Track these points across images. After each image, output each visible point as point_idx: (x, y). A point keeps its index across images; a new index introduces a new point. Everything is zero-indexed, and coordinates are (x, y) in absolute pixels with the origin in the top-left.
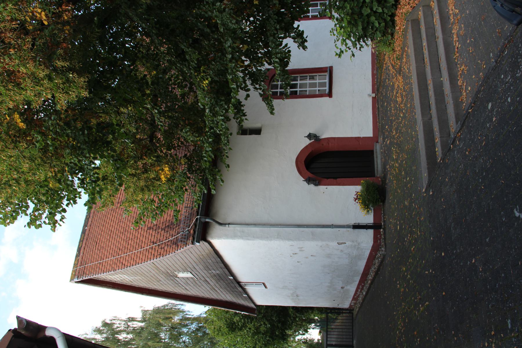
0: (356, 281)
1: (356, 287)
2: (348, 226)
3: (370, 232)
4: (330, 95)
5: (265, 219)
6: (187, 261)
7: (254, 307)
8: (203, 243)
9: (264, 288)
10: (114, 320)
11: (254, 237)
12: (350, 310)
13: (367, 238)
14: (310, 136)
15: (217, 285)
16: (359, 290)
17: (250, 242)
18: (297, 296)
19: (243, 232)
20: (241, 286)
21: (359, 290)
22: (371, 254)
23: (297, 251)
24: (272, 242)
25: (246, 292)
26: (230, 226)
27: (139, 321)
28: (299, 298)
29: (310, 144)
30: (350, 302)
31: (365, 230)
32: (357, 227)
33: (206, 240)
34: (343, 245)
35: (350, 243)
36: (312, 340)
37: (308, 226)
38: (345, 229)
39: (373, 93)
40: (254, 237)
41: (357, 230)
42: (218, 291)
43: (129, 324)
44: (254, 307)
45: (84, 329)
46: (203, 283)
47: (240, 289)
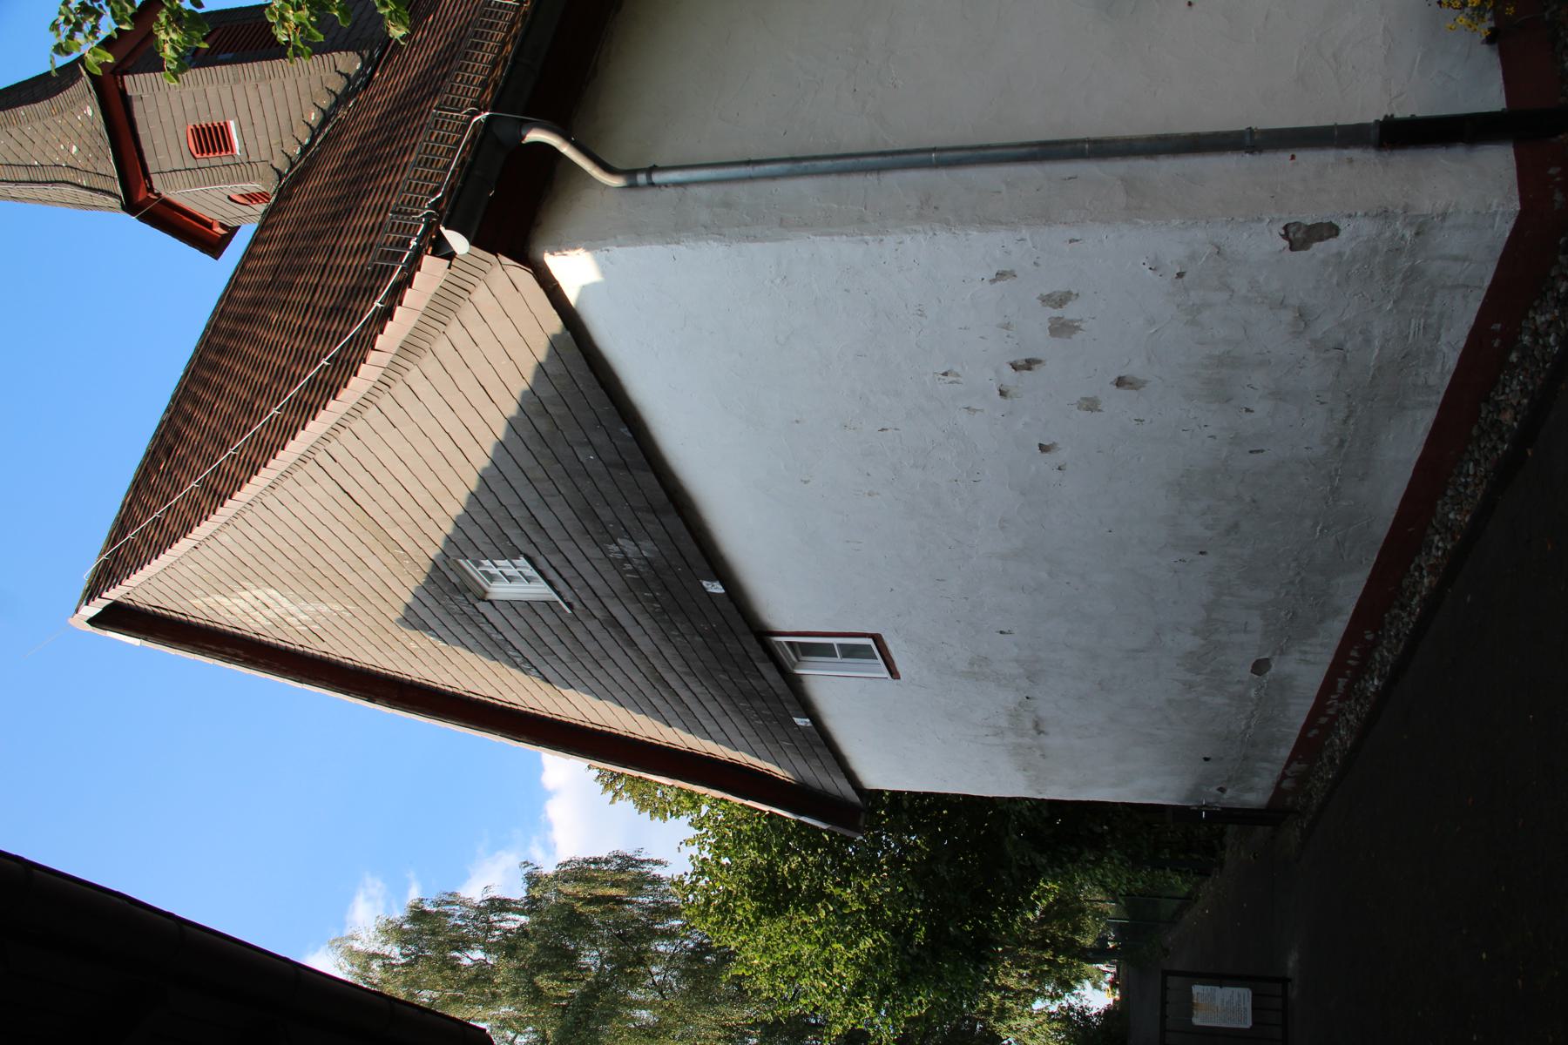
0: (1337, 612)
1: (1328, 658)
5: (856, 135)
6: (255, 341)
7: (856, 799)
9: (886, 674)
10: (448, 903)
11: (786, 223)
12: (1272, 815)
13: (1475, 199)
15: (668, 652)
16: (1341, 682)
17: (762, 255)
18: (1038, 728)
19: (727, 205)
20: (771, 654)
21: (1341, 682)
22: (1478, 335)
23: (1037, 339)
24: (890, 240)
25: (808, 709)
26: (657, 178)
27: (521, 912)
28: (1043, 739)
30: (1278, 769)
31: (1459, 151)
32: (1398, 134)
35: (1368, 228)
36: (1082, 1013)
38: (1329, 155)
40: (782, 223)
41: (1403, 161)
42: (694, 706)
43: (493, 918)
44: (856, 799)
45: (339, 933)
46: (601, 635)
47: (772, 676)
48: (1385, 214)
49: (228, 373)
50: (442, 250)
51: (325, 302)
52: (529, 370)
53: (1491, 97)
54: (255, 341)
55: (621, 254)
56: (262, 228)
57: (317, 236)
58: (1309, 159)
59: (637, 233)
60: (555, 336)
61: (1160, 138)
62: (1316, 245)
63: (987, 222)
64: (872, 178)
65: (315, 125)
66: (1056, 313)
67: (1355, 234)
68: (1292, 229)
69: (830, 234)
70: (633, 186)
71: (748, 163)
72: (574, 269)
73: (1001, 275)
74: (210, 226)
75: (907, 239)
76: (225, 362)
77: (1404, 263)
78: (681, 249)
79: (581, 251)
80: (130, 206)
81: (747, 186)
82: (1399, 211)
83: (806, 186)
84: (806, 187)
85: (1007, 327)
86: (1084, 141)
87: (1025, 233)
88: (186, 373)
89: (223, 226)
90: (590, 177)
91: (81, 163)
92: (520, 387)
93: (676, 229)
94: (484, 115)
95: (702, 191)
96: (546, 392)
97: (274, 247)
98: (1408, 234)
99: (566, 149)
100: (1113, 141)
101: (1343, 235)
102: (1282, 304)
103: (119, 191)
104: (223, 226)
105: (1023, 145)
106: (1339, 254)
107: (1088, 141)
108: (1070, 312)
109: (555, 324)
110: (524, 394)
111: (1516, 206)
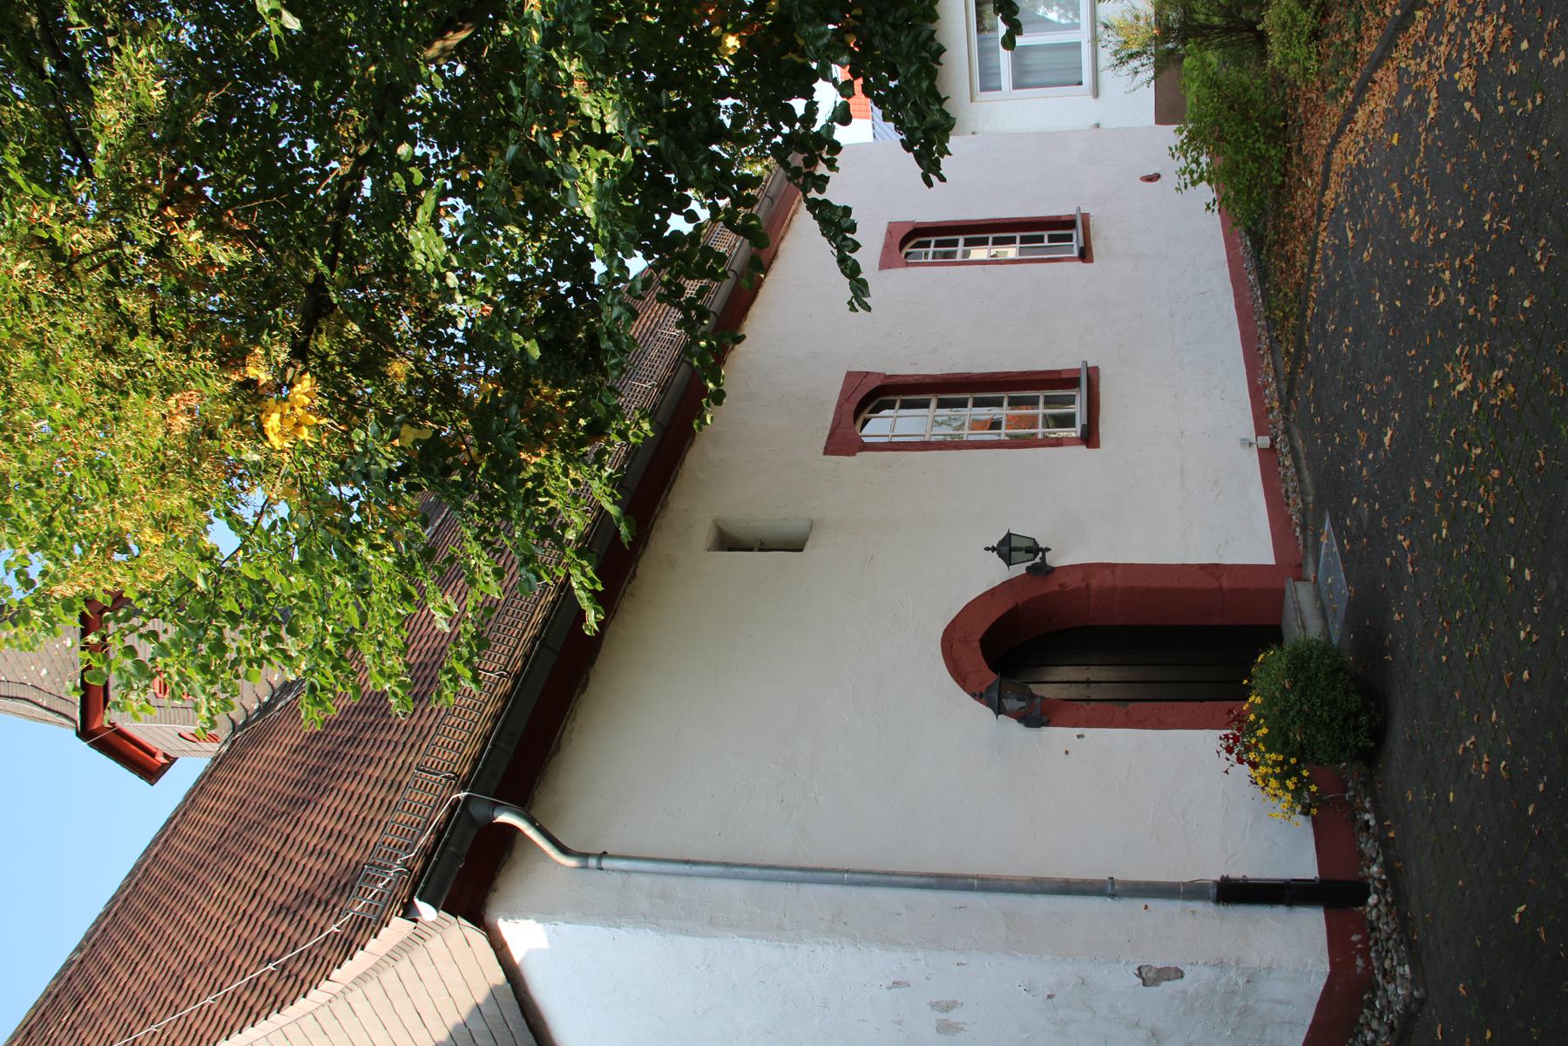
2: (1192, 891)
3: (1311, 922)
4: (1090, 438)
5: (781, 849)
6: (192, 907)
8: (461, 932)
11: (716, 922)
13: (1295, 949)
14: (1007, 549)
17: (692, 946)
26: (606, 863)
29: (1008, 585)
31: (1281, 910)
32: (1233, 892)
33: (477, 917)
34: (1166, 986)
35: (1208, 974)
37: (987, 885)
38: (1176, 906)
39: (1260, 431)
41: (1239, 914)
48: (1221, 964)
49: (158, 932)
50: (409, 912)
51: (275, 895)
52: (466, 1007)
53: (1304, 865)
54: (192, 907)
55: (569, 930)
56: (208, 777)
57: (272, 815)
58: (1160, 906)
59: (583, 912)
60: (496, 986)
61: (1036, 880)
62: (1164, 984)
63: (888, 941)
64: (792, 887)
65: (277, 686)
66: (944, 1016)
67: (1197, 977)
68: (1144, 971)
69: (753, 937)
70: (585, 867)
71: (687, 862)
72: (524, 935)
73: (896, 984)
74: (153, 755)
75: (819, 949)
76: (155, 917)
77: (1238, 1002)
78: (622, 934)
79: (532, 922)
80: (85, 733)
81: (683, 880)
82: (1233, 963)
83: (736, 888)
84: (735, 889)
85: (900, 1023)
86: (973, 877)
87: (919, 954)
88: (106, 913)
89: (166, 756)
90: (543, 851)
91: (46, 685)
92: (453, 1019)
93: (617, 914)
94: (462, 795)
95: (645, 881)
96: (478, 1026)
97: (222, 806)
98: (1241, 981)
99: (530, 832)
100: (998, 879)
101: (1186, 977)
102: (1137, 1025)
103: (77, 716)
104: (166, 756)
105: (922, 876)
106: (1184, 992)
107: (977, 877)
108: (954, 1016)
109: (498, 976)
110: (457, 1026)
111: (1327, 968)
